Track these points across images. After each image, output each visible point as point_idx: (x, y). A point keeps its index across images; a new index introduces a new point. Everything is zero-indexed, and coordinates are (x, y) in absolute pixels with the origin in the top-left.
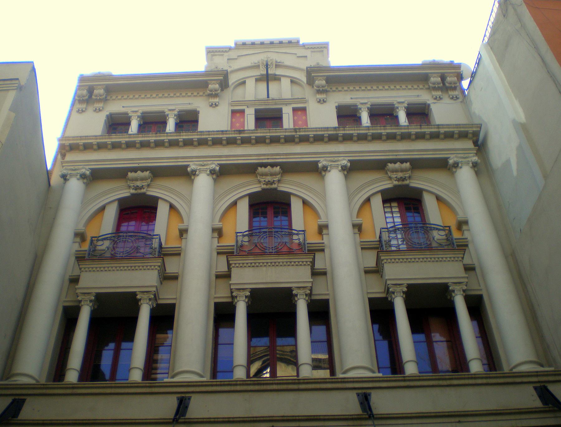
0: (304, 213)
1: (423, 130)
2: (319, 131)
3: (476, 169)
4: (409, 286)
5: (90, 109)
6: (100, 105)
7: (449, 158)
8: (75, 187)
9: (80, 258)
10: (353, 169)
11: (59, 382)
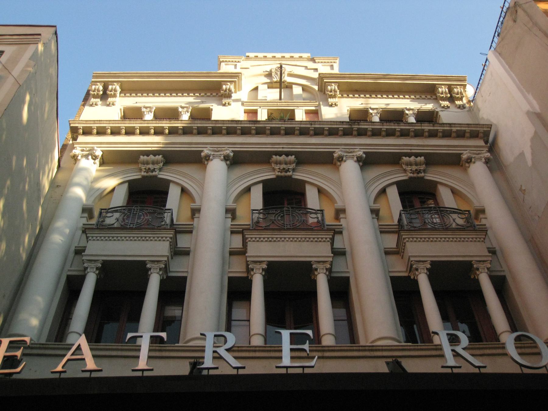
0: (319, 201)
1: (435, 128)
2: (334, 124)
3: (488, 165)
4: (433, 263)
7: (462, 154)
9: (85, 230)
10: (367, 162)
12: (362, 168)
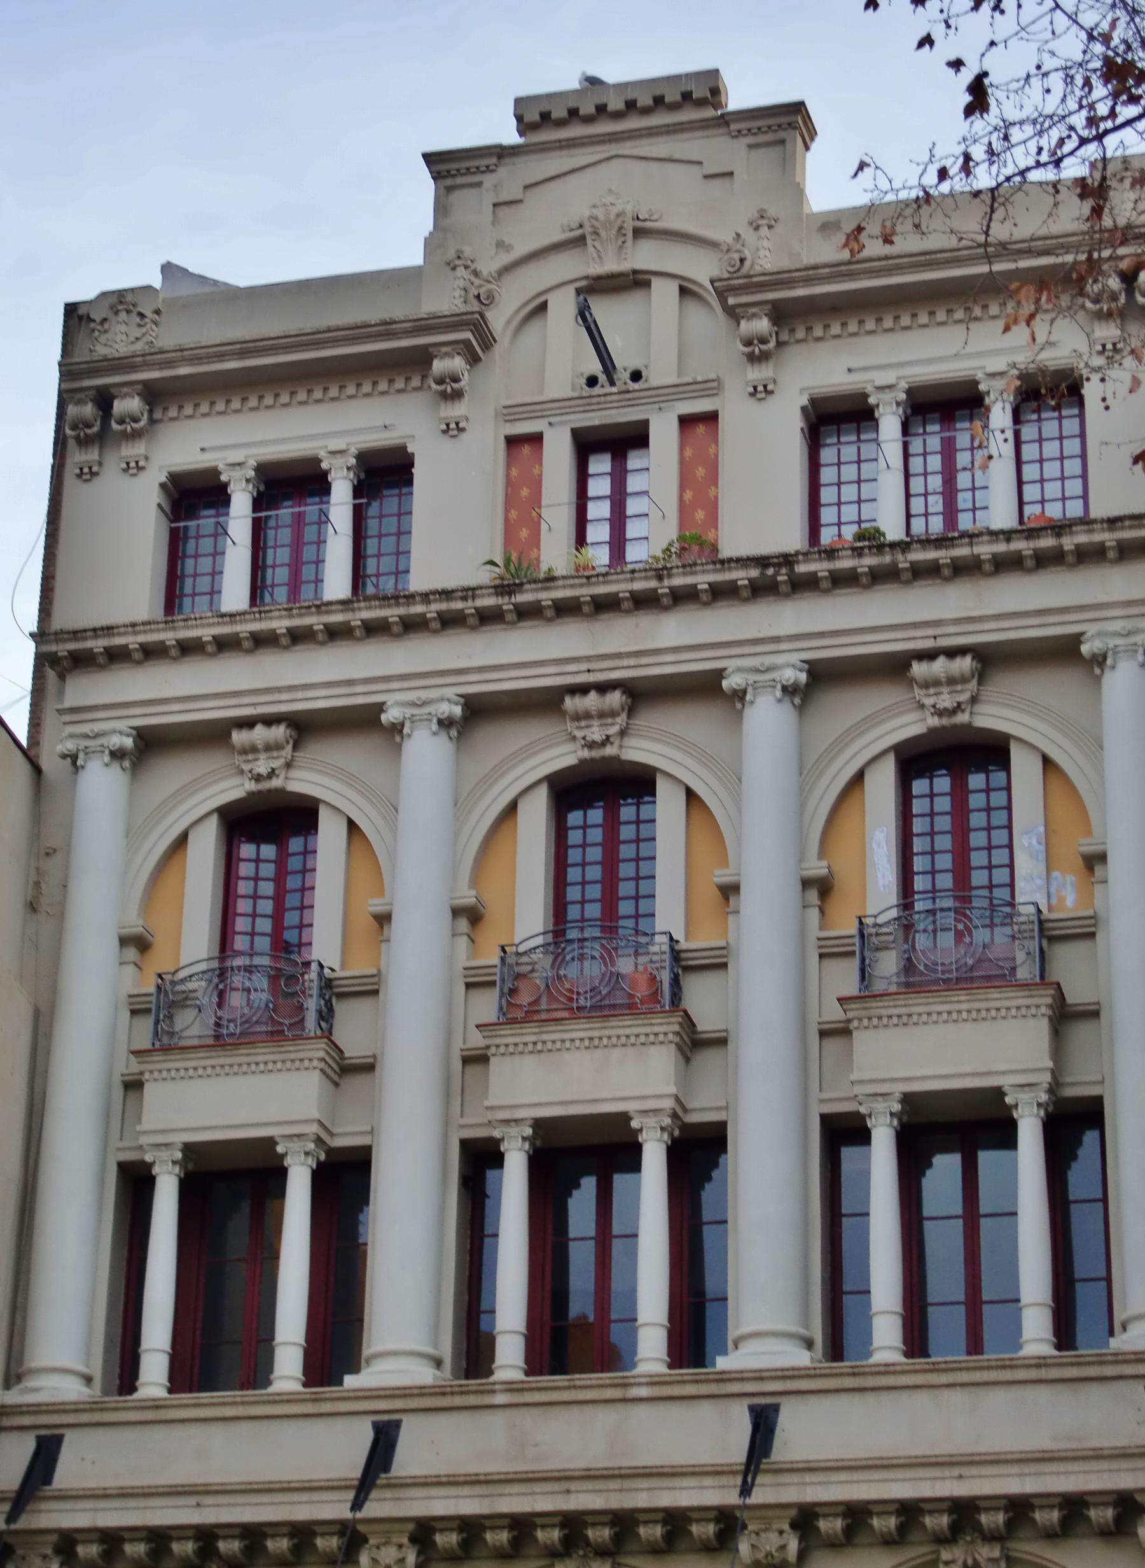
5: (113, 462)
6: (136, 449)
8: (101, 788)
11: (560, 1380)
12: (801, 709)
